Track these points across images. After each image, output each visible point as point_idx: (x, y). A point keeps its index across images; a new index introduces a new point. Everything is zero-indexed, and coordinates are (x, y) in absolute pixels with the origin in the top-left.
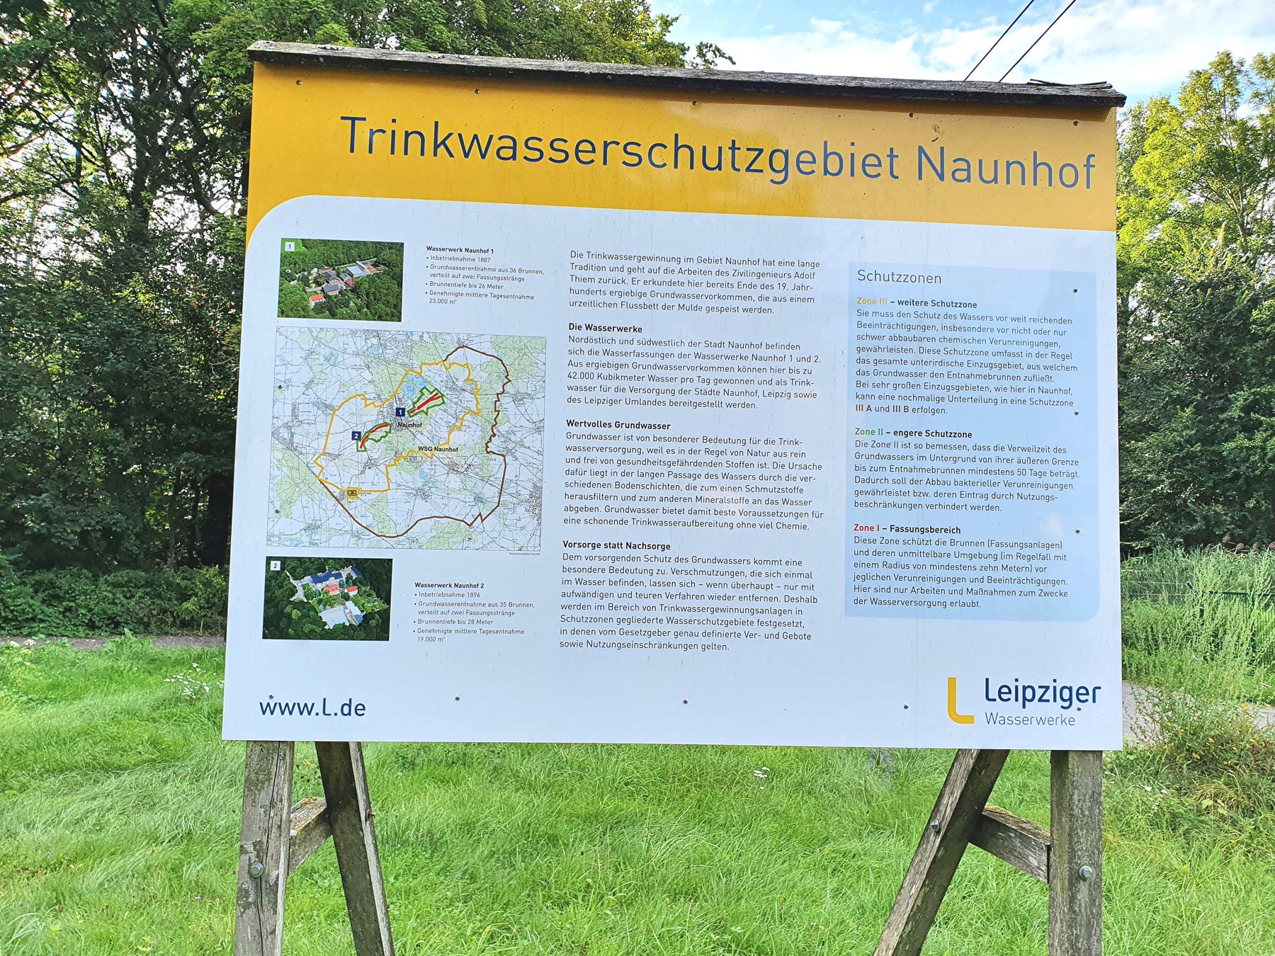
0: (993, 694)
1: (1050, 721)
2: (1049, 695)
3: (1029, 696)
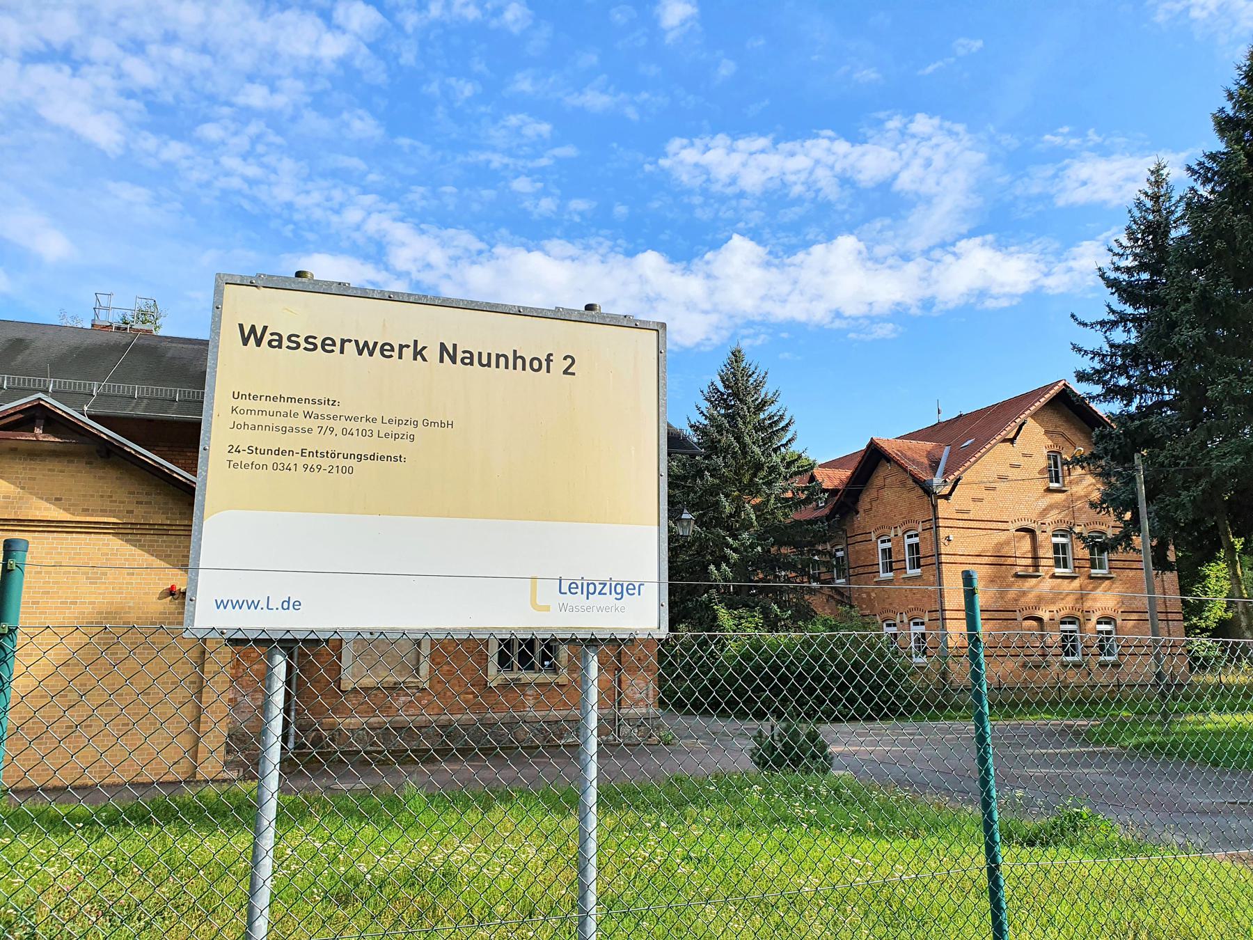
0: (565, 589)
1: (607, 609)
2: (606, 590)
3: (591, 590)
